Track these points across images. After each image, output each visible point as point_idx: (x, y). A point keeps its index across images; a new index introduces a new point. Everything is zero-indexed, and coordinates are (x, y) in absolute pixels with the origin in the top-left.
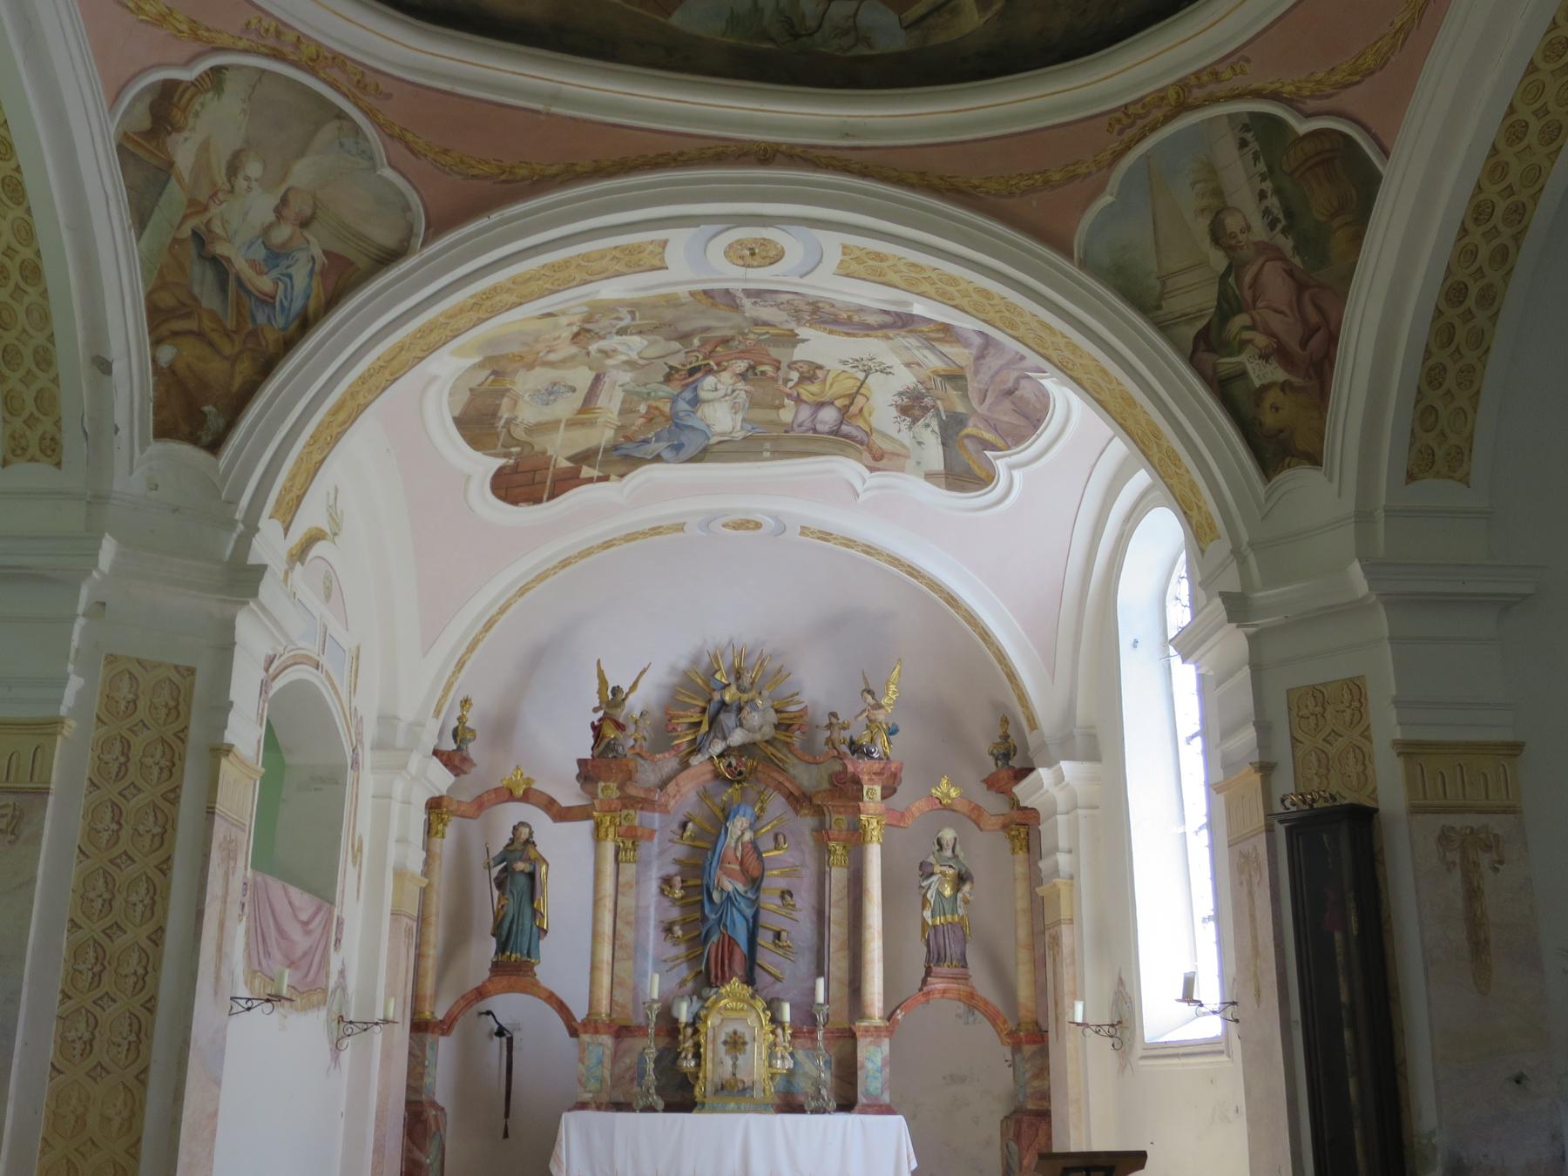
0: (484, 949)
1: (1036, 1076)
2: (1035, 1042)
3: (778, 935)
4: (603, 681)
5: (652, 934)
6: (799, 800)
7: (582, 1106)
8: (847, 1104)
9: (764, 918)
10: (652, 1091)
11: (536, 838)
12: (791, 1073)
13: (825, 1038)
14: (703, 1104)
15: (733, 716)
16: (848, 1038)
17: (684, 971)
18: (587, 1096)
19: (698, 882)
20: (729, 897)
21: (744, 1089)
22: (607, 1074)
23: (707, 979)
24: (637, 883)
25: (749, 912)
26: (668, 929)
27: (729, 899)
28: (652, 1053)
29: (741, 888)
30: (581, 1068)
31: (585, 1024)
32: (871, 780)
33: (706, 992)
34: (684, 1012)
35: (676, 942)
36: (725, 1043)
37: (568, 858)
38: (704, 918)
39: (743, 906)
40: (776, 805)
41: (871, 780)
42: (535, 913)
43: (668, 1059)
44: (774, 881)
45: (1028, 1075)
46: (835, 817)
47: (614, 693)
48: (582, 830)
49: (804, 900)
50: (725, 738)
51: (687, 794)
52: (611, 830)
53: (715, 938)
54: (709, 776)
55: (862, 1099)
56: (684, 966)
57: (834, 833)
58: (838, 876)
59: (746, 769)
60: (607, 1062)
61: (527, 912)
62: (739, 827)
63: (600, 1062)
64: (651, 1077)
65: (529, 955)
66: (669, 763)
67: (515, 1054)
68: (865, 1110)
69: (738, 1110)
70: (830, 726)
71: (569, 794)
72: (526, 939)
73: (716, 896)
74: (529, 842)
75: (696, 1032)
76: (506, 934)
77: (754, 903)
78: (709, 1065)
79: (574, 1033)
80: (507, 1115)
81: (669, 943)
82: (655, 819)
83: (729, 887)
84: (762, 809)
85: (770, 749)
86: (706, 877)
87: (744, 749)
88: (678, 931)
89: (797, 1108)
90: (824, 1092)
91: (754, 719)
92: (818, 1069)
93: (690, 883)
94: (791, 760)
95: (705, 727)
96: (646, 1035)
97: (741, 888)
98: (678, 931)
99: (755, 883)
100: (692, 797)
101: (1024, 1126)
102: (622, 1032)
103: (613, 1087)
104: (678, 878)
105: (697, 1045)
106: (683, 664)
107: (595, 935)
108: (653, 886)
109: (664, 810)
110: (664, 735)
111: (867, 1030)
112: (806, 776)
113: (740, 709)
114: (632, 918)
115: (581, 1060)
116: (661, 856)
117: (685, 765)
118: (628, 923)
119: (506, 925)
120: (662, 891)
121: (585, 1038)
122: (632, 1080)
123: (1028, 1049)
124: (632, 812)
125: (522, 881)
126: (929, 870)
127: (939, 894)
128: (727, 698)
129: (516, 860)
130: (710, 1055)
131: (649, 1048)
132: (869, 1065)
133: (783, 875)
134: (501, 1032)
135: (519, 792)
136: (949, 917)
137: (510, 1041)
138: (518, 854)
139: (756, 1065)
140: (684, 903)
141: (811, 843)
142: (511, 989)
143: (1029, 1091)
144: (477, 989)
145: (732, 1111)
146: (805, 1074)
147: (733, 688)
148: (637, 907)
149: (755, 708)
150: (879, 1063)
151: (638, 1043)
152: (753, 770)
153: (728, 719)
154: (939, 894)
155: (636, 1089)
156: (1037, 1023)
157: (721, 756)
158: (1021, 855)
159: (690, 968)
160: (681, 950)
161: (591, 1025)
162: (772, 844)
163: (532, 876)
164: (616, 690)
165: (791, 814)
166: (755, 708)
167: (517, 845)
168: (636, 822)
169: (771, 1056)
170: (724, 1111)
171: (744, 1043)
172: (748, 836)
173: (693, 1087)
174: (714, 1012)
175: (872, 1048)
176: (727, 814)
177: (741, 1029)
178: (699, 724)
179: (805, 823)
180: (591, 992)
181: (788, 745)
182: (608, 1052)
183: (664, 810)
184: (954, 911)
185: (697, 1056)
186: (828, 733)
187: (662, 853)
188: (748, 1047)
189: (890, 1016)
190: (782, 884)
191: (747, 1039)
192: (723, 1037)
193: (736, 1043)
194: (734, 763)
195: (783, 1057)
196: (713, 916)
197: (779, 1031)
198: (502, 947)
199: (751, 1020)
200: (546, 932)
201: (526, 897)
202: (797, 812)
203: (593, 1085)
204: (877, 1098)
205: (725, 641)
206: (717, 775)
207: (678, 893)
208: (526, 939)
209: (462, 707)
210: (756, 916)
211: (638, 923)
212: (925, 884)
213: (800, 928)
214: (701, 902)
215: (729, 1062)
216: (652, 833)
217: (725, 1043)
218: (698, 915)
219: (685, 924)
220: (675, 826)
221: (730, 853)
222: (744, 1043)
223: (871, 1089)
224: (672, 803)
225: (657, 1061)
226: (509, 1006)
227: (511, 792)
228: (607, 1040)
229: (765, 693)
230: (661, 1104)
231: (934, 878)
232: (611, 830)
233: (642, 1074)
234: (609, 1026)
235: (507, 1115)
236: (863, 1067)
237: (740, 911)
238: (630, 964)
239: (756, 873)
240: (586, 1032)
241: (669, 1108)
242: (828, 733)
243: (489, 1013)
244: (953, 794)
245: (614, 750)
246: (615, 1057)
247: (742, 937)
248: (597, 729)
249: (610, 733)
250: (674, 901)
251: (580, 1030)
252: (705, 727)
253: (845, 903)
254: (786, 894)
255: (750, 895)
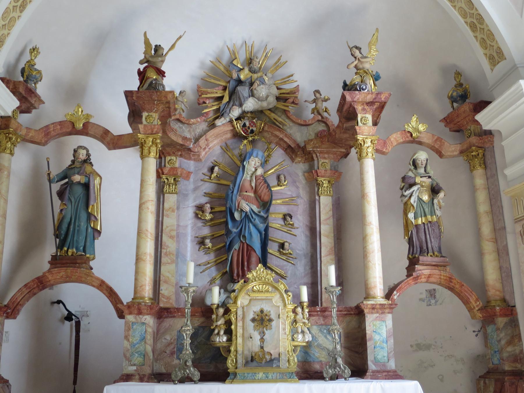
0: (50, 249)
1: (510, 343)
2: (506, 315)
3: (282, 246)
4: (147, 43)
5: (189, 246)
6: (293, 151)
7: (127, 378)
8: (359, 371)
9: (273, 234)
10: (189, 363)
11: (93, 160)
12: (309, 345)
13: (338, 316)
14: (235, 374)
15: (247, 89)
16: (356, 315)
17: (213, 272)
18: (132, 369)
19: (223, 209)
20: (247, 216)
21: (271, 360)
22: (149, 349)
23: (232, 274)
24: (178, 208)
25: (262, 227)
26: (201, 242)
27: (247, 217)
28: (189, 330)
29: (255, 209)
30: (126, 344)
31: (129, 306)
32: (364, 109)
33: (230, 286)
34: (216, 296)
35: (207, 251)
36: (253, 320)
37: (122, 182)
38: (228, 232)
39: (257, 221)
40: (278, 155)
41: (364, 109)
42: (90, 216)
43: (203, 335)
44: (278, 208)
45: (503, 342)
46: (321, 161)
47: (156, 50)
48: (131, 155)
49: (300, 221)
50: (241, 105)
51: (213, 146)
52: (154, 149)
53: (236, 247)
54: (229, 135)
55: (372, 366)
56: (213, 269)
57: (321, 171)
58: (325, 203)
59: (259, 129)
60: (149, 338)
61: (83, 216)
62: (253, 164)
63: (143, 339)
64: (188, 351)
65: (84, 251)
66: (201, 126)
67: (81, 334)
68: (376, 376)
69: (266, 380)
70: (314, 101)
71: (119, 122)
72: (82, 238)
73: (237, 215)
74: (87, 161)
75: (227, 311)
76: (63, 237)
77: (265, 220)
78: (240, 340)
79: (121, 315)
80: (75, 382)
81: (202, 253)
82: (190, 165)
83: (247, 209)
84: (269, 156)
85: (273, 115)
86: (229, 202)
87: (258, 114)
88: (209, 243)
89: (318, 376)
90: (340, 361)
91: (262, 91)
92: (330, 341)
93: (217, 209)
94: (288, 122)
95: (226, 99)
96: (183, 316)
97: (255, 209)
98: (209, 243)
99: (266, 205)
100: (218, 150)
101: (507, 384)
102: (163, 313)
103: (156, 360)
104: (208, 205)
105: (229, 323)
106: (208, 60)
107: (140, 233)
108: (190, 212)
109: (198, 160)
110: (197, 108)
111: (373, 308)
112: (299, 135)
113: (251, 84)
114: (174, 233)
115: (126, 338)
116: (194, 191)
117: (212, 126)
118: (171, 237)
119: (65, 226)
120: (196, 215)
121: (130, 318)
122: (172, 353)
123: (501, 321)
124: (174, 158)
125: (79, 191)
126: (411, 181)
127: (420, 200)
128: (242, 77)
129: (74, 174)
130: (240, 331)
131: (186, 327)
132: (377, 337)
133: (284, 204)
134: (69, 317)
135: (80, 126)
136: (429, 218)
137: (78, 324)
138: (76, 170)
139: (284, 339)
140: (213, 224)
141: (304, 182)
142: (68, 280)
143: (505, 355)
144: (38, 278)
145: (260, 381)
146: (319, 346)
147: (246, 70)
148: (178, 226)
149: (263, 82)
150: (384, 335)
151: (177, 323)
152: (261, 132)
153: (243, 91)
154: (420, 200)
155: (176, 362)
156: (504, 300)
157: (238, 119)
158: (479, 172)
159: (218, 270)
160: (211, 257)
161: (136, 307)
162: (275, 183)
163: (86, 186)
164: (158, 48)
165: (288, 161)
166: (263, 82)
167: (77, 164)
168: (177, 165)
169: (294, 332)
170: (254, 381)
171: (270, 320)
172: (260, 172)
173: (226, 359)
174: (242, 294)
175: (378, 323)
176: (243, 158)
177: (266, 308)
178: (220, 98)
179: (299, 168)
180: (136, 279)
181: (285, 112)
182: (150, 330)
183: (198, 160)
184: (433, 213)
185: (229, 332)
186: (313, 105)
187: (196, 189)
188: (274, 324)
189: (388, 296)
190: (284, 209)
191: (273, 316)
192: (251, 316)
193: (262, 320)
194: (247, 124)
195: (303, 332)
196: (235, 230)
197: (299, 310)
198: (60, 247)
199: (276, 299)
200: (99, 233)
201: (82, 205)
202: (293, 160)
203: (137, 359)
204: (384, 365)
205: (239, 42)
206: (237, 136)
207: (208, 217)
208: (82, 238)
209: (31, 53)
210: (266, 229)
211: (178, 237)
212: (407, 193)
213: (299, 242)
214: (226, 223)
215: (257, 337)
216: (189, 173)
217: (253, 320)
218: (223, 232)
219: (213, 238)
220: (205, 170)
221: (247, 184)
222: (270, 320)
223: (379, 357)
224: (203, 153)
225: (193, 337)
226: (76, 295)
227: (73, 124)
228: (149, 320)
229: (269, 75)
230: (197, 375)
231: (415, 188)
232: (154, 149)
233: (180, 349)
234: (151, 308)
235: (75, 382)
236: (371, 339)
237: (255, 226)
238: (173, 267)
239: (266, 198)
240: (130, 313)
241: (206, 378)
242: (313, 105)
243: (59, 302)
244: (421, 128)
245: (155, 88)
246: (157, 335)
247: (257, 245)
248: (142, 75)
249: (153, 75)
250: (205, 222)
251: (126, 311)
252: (226, 99)
253: (331, 221)
254: (286, 217)
255: (262, 214)
